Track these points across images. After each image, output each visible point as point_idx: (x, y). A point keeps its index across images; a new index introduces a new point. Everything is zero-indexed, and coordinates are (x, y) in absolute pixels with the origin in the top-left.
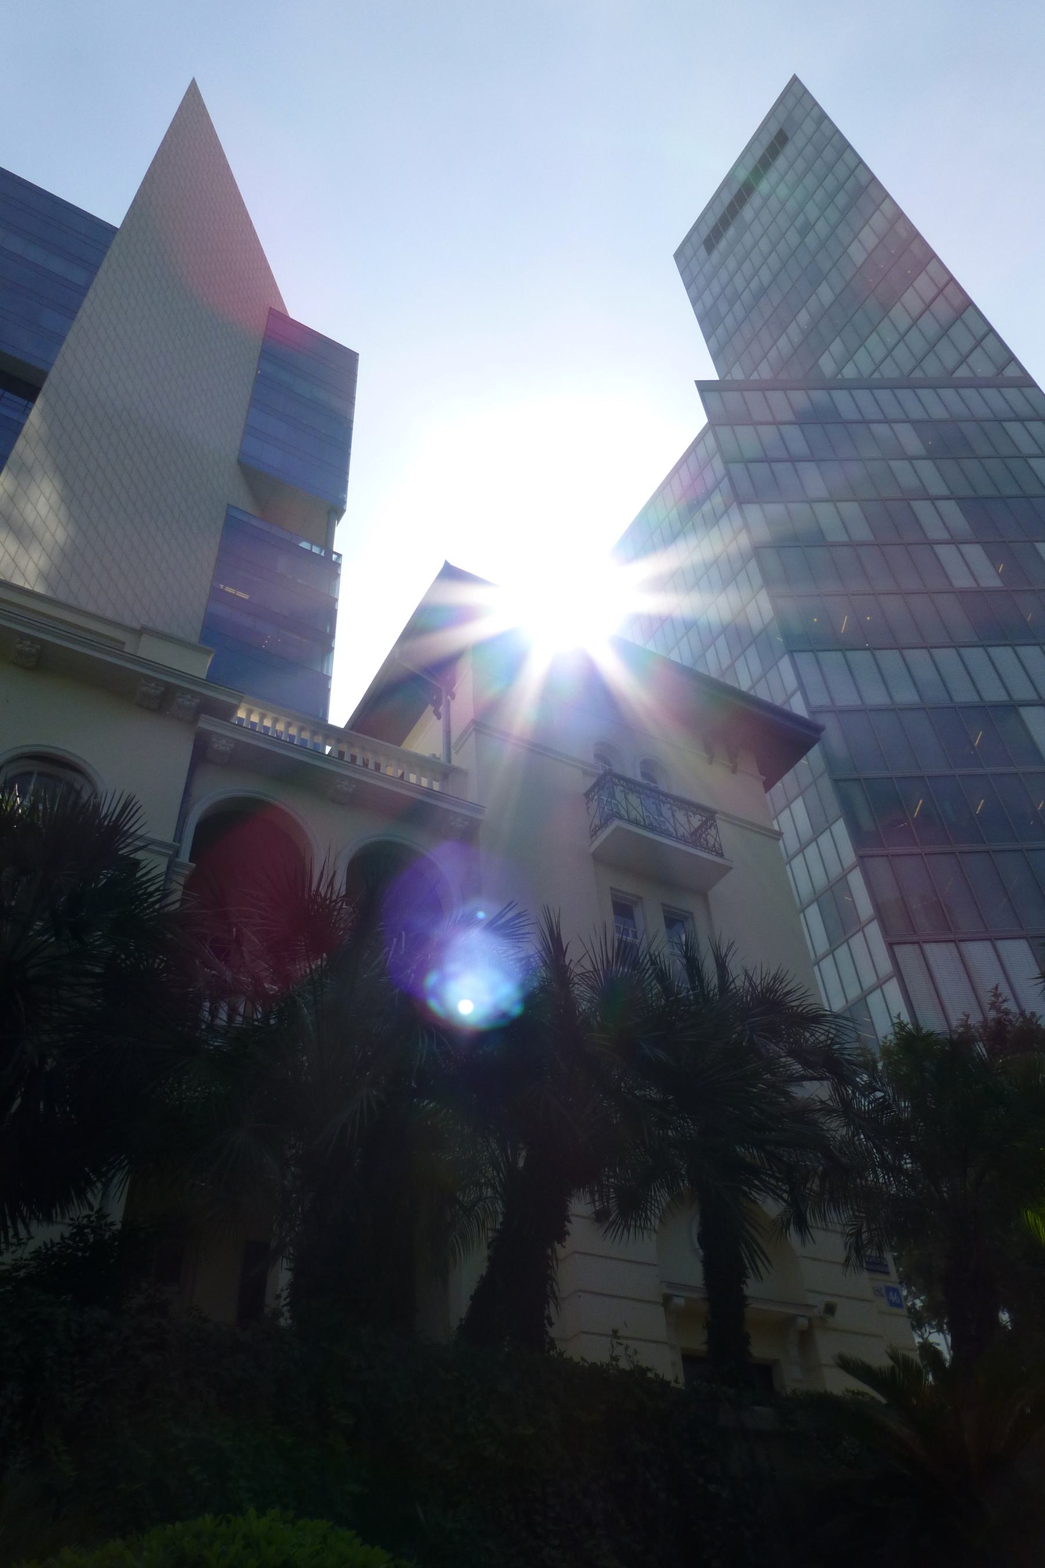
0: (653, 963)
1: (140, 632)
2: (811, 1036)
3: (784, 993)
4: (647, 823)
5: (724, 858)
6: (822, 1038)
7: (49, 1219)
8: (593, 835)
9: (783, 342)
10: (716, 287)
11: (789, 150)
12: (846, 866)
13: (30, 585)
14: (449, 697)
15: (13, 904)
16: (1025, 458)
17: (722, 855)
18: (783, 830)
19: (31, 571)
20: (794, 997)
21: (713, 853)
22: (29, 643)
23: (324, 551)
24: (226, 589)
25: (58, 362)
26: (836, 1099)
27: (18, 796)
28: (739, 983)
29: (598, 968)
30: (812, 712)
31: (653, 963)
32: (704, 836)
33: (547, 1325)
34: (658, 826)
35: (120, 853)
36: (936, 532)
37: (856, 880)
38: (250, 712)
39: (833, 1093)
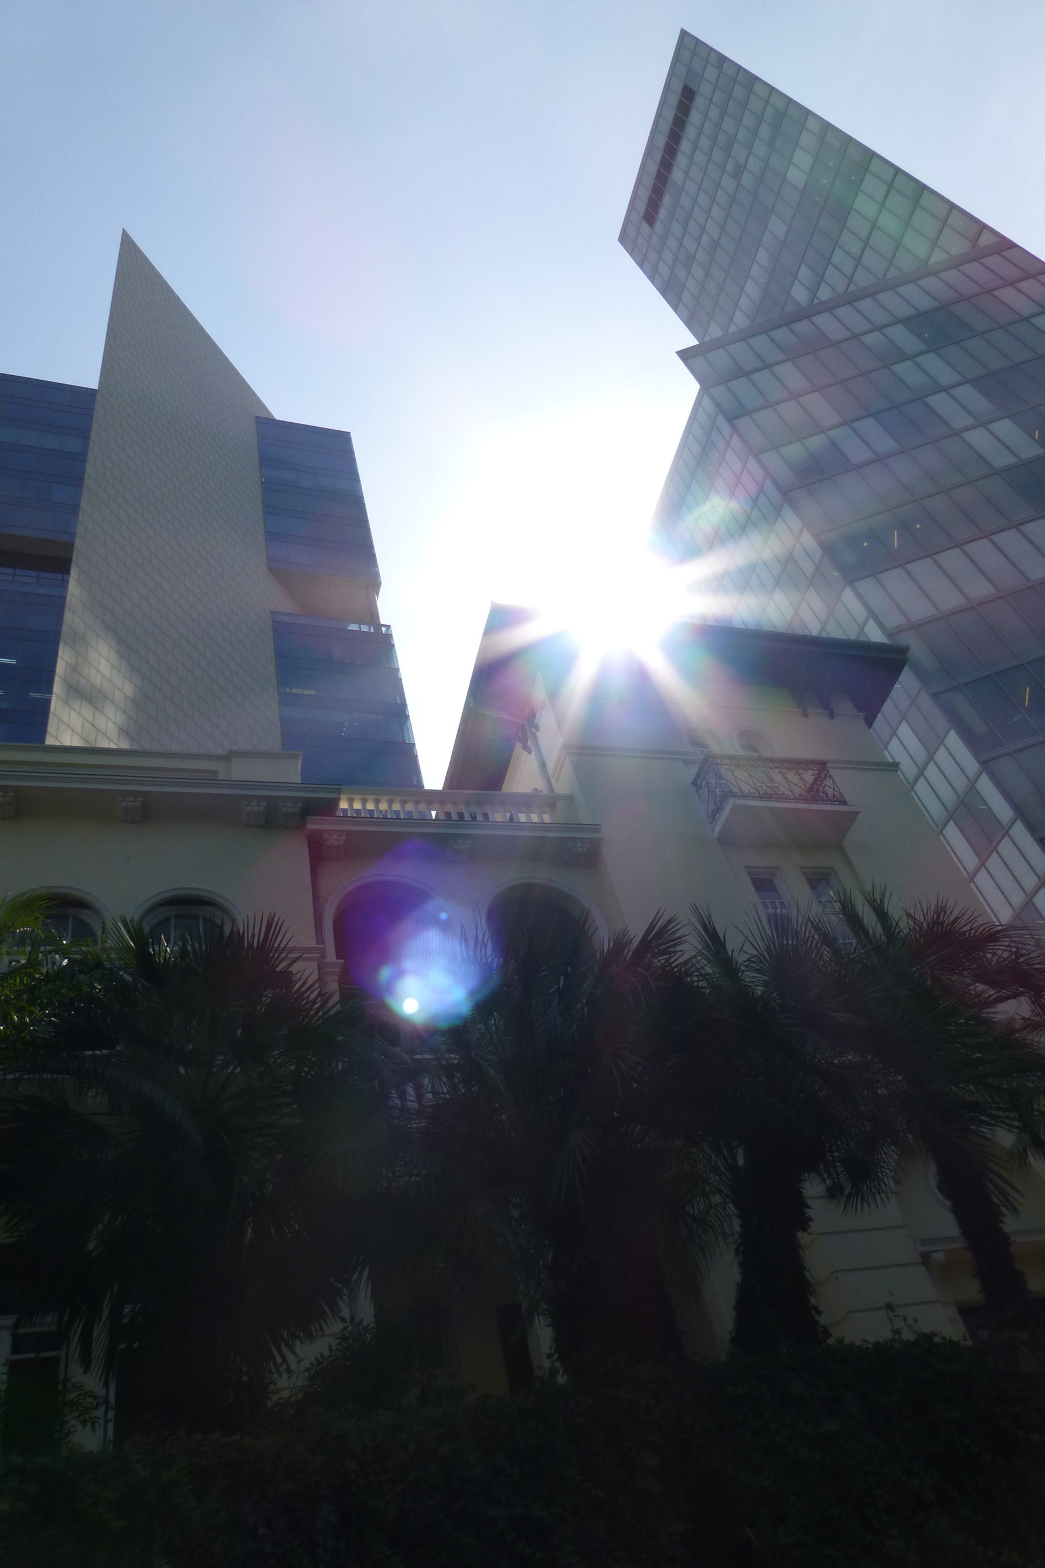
0: (817, 929)
1: (228, 757)
2: (993, 956)
3: (951, 922)
4: (761, 793)
5: (847, 805)
6: (1006, 955)
7: (310, 1336)
8: (712, 821)
9: (750, 288)
10: (668, 256)
11: (699, 102)
12: (971, 777)
13: (115, 743)
14: (533, 730)
15: (190, 1048)
16: (1027, 319)
17: (844, 803)
18: (897, 760)
19: (111, 729)
20: (962, 924)
21: (835, 803)
22: (131, 798)
23: (372, 627)
24: (293, 692)
25: (80, 530)
26: (1038, 1012)
27: (167, 946)
28: (903, 925)
29: (761, 950)
30: (890, 635)
31: (817, 929)
32: (821, 789)
33: (815, 1315)
34: (773, 793)
35: (278, 969)
36: (960, 420)
37: (986, 786)
38: (351, 801)
39: (1033, 1008)
